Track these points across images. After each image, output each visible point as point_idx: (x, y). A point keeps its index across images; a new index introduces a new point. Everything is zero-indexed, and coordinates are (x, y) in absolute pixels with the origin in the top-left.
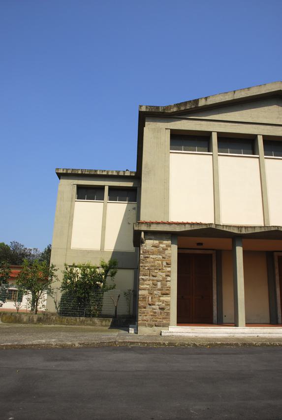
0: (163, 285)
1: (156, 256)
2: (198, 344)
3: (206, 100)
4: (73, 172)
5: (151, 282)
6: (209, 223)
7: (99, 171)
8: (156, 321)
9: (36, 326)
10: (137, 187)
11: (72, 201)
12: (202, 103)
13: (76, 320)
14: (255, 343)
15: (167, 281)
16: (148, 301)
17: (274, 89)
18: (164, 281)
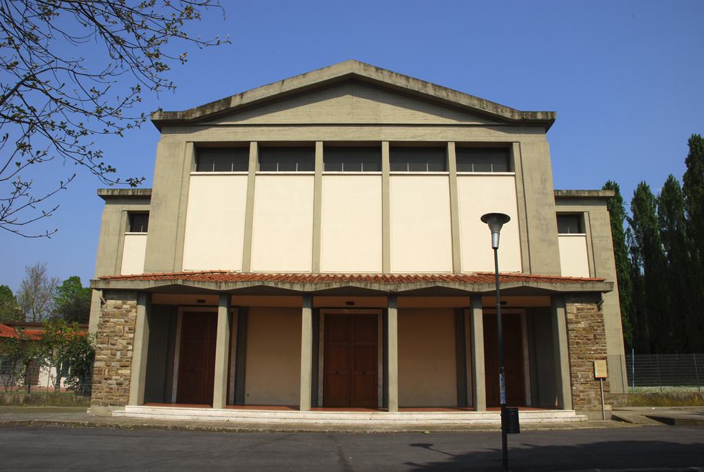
0: (123, 355)
2: (121, 425)
8: (112, 399)
9: (24, 407)
12: (235, 102)
14: (188, 427)
16: (104, 373)
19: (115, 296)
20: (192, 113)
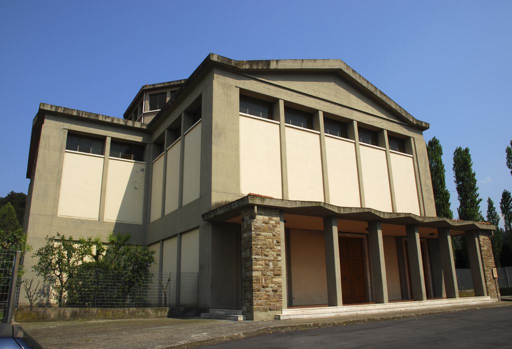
0: (275, 265)
1: (267, 234)
2: (336, 323)
3: (277, 63)
4: (66, 112)
5: (264, 262)
6: (319, 201)
7: (101, 116)
10: (146, 144)
11: (61, 151)
12: (273, 66)
13: (124, 312)
15: (278, 261)
16: (262, 283)
17: (331, 66)
18: (275, 260)
19: (263, 213)
20: (243, 65)
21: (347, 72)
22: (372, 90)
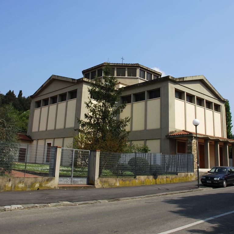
12: (185, 80)
21: (204, 80)
22: (211, 87)
